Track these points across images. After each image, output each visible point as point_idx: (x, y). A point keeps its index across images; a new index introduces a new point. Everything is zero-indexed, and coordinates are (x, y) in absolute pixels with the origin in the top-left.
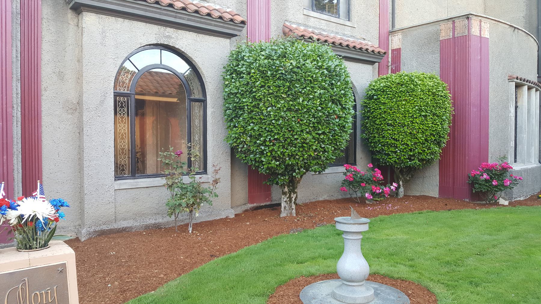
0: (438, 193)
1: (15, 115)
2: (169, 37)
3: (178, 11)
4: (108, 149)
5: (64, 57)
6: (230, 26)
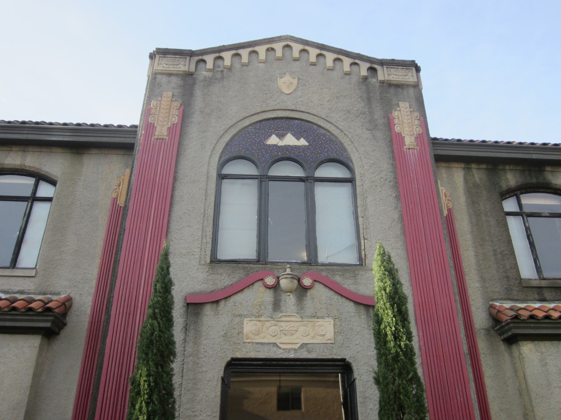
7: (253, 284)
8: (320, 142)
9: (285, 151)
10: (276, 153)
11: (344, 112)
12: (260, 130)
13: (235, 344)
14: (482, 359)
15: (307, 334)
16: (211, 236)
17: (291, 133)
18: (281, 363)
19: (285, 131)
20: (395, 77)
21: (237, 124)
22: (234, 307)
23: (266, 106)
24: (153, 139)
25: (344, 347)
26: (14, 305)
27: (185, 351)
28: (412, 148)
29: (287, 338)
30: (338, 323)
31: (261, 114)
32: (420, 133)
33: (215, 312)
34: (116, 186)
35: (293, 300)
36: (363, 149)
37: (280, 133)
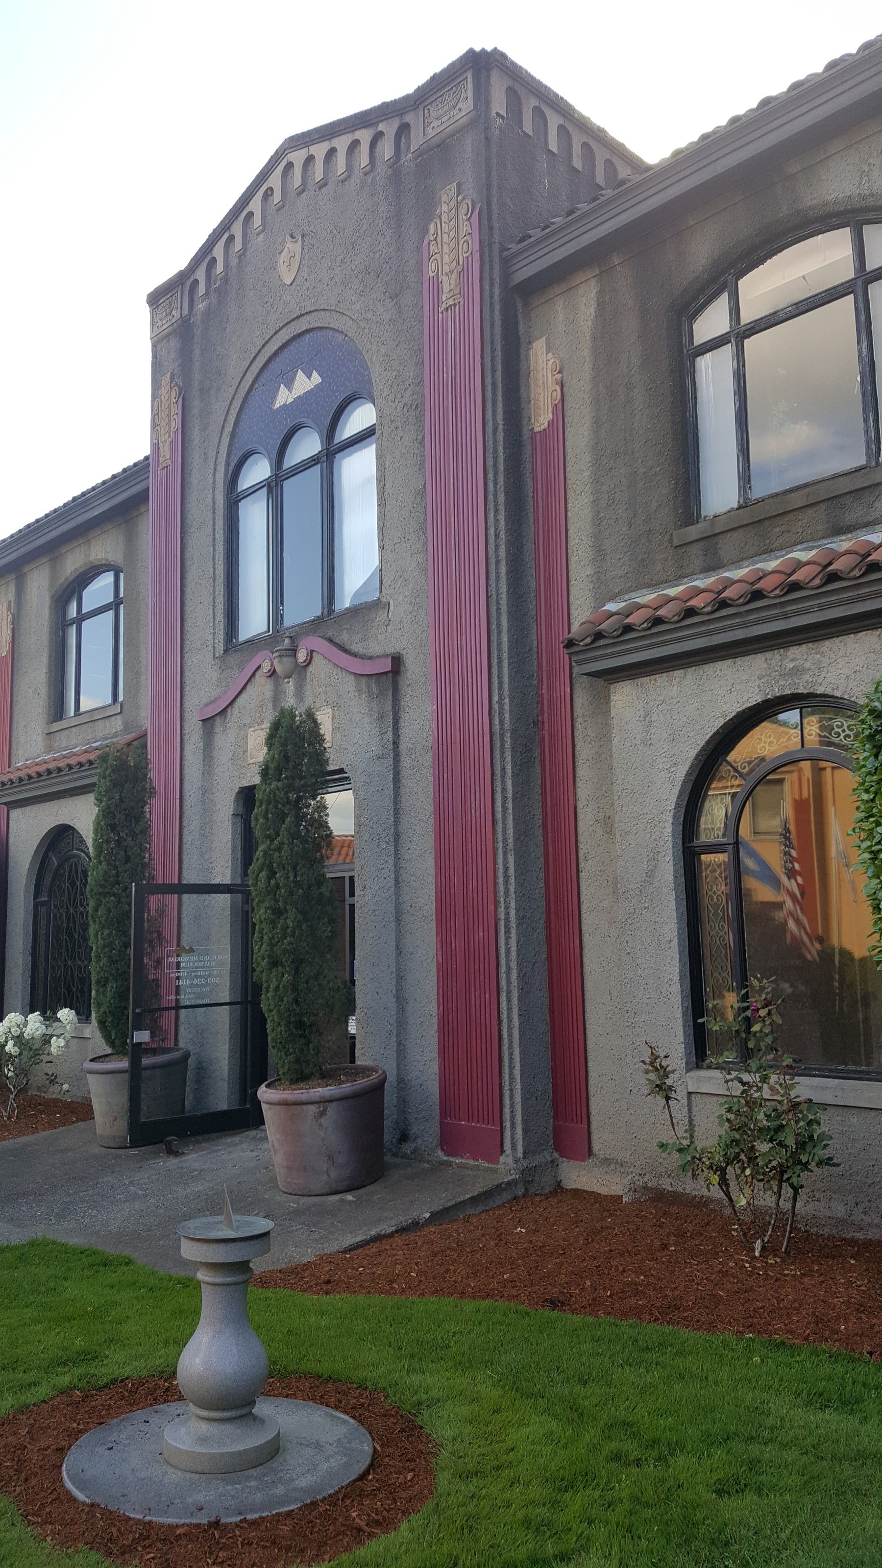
2: (797, 671)
3: (783, 599)
4: (668, 985)
6: (728, 623)
26: (793, 578)
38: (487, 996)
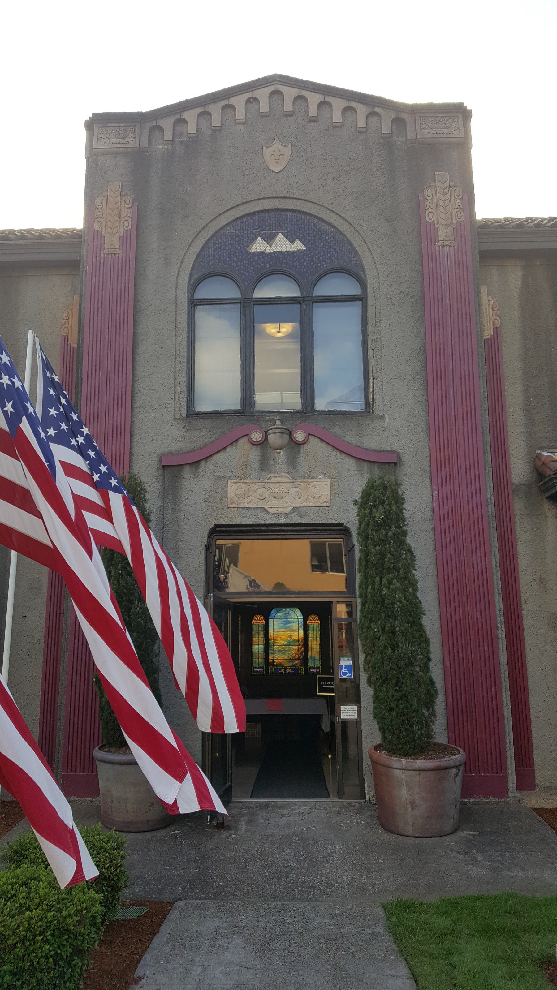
0: (209, 723)
1: (500, 637)
5: (545, 558)
7: (236, 441)
8: (322, 244)
9: (274, 261)
10: (262, 265)
11: (355, 195)
12: (242, 231)
13: (218, 509)
14: (518, 521)
15: (300, 496)
16: (185, 384)
17: (282, 233)
18: (271, 528)
19: (274, 230)
20: (432, 132)
21: (210, 225)
22: (216, 468)
23: (248, 193)
24: (102, 255)
25: (342, 511)
27: (163, 518)
28: (447, 245)
29: (276, 501)
30: (336, 483)
31: (241, 207)
32: (461, 220)
33: (195, 475)
34: (64, 319)
35: (283, 457)
36: (379, 251)
37: (267, 235)
38: (493, 688)
